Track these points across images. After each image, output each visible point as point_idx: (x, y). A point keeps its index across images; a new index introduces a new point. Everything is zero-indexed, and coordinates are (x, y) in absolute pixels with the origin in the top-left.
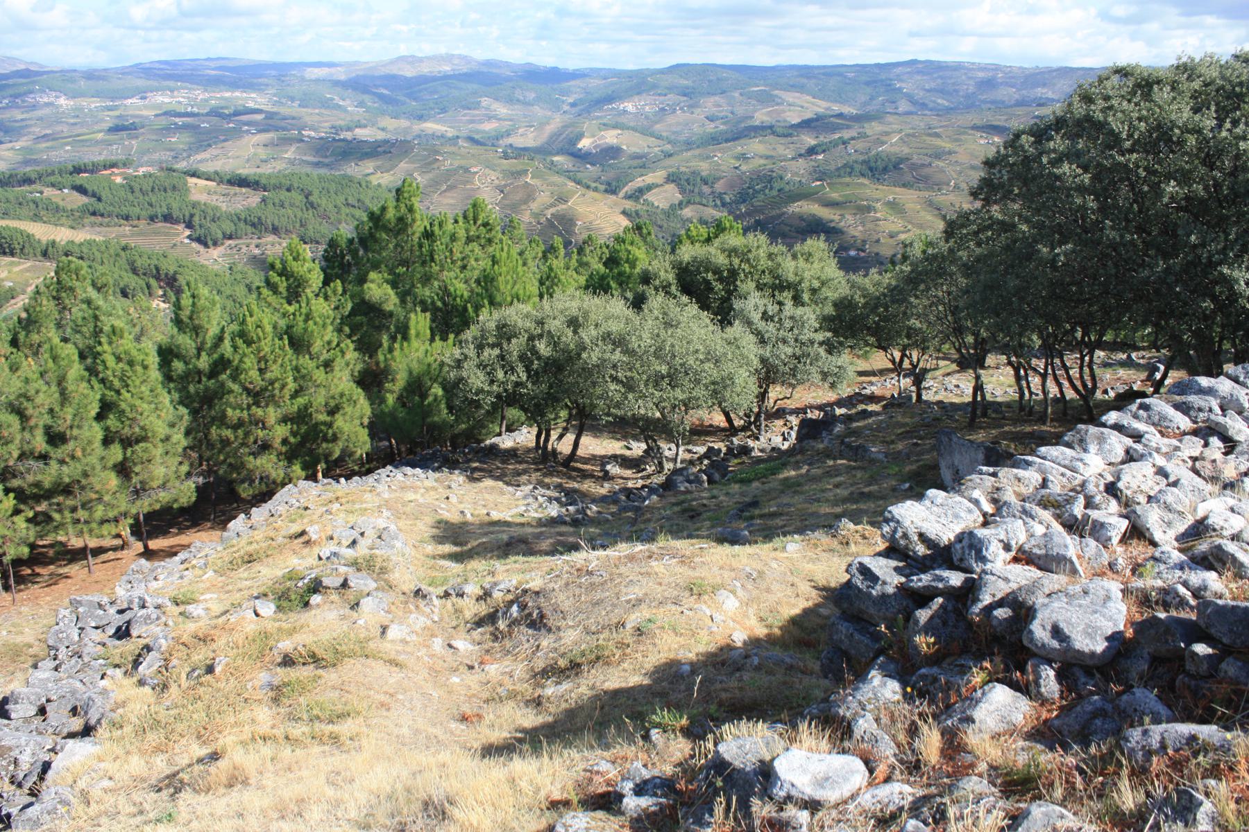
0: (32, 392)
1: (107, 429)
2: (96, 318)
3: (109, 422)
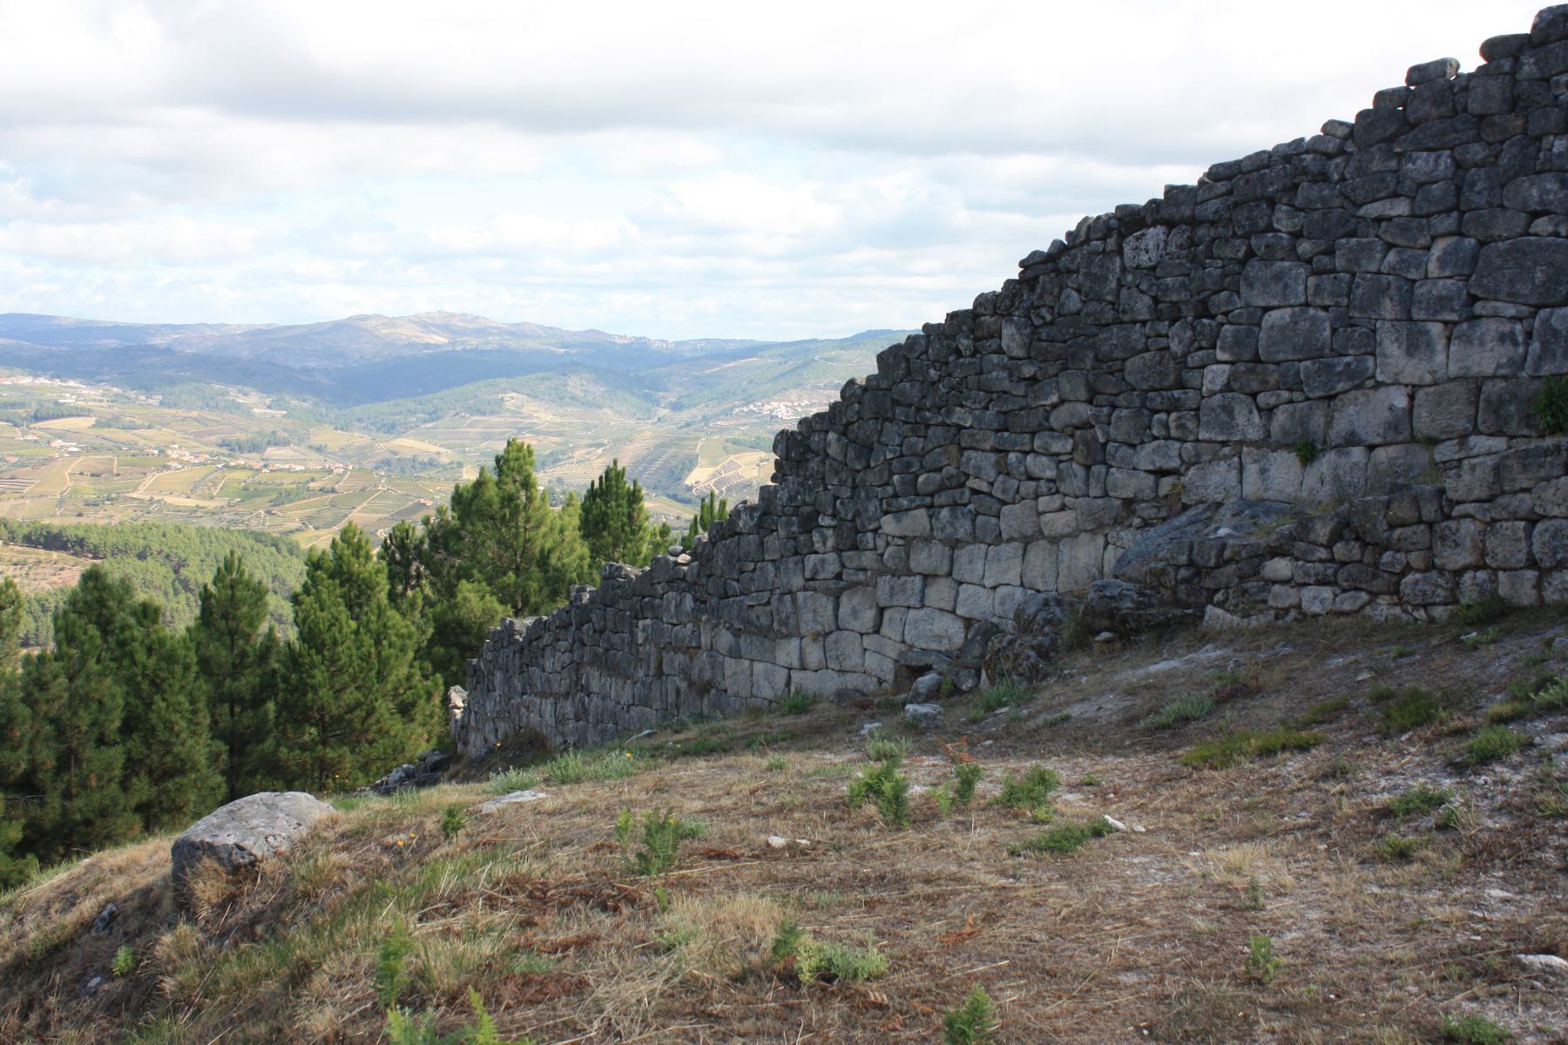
1: (128, 752)
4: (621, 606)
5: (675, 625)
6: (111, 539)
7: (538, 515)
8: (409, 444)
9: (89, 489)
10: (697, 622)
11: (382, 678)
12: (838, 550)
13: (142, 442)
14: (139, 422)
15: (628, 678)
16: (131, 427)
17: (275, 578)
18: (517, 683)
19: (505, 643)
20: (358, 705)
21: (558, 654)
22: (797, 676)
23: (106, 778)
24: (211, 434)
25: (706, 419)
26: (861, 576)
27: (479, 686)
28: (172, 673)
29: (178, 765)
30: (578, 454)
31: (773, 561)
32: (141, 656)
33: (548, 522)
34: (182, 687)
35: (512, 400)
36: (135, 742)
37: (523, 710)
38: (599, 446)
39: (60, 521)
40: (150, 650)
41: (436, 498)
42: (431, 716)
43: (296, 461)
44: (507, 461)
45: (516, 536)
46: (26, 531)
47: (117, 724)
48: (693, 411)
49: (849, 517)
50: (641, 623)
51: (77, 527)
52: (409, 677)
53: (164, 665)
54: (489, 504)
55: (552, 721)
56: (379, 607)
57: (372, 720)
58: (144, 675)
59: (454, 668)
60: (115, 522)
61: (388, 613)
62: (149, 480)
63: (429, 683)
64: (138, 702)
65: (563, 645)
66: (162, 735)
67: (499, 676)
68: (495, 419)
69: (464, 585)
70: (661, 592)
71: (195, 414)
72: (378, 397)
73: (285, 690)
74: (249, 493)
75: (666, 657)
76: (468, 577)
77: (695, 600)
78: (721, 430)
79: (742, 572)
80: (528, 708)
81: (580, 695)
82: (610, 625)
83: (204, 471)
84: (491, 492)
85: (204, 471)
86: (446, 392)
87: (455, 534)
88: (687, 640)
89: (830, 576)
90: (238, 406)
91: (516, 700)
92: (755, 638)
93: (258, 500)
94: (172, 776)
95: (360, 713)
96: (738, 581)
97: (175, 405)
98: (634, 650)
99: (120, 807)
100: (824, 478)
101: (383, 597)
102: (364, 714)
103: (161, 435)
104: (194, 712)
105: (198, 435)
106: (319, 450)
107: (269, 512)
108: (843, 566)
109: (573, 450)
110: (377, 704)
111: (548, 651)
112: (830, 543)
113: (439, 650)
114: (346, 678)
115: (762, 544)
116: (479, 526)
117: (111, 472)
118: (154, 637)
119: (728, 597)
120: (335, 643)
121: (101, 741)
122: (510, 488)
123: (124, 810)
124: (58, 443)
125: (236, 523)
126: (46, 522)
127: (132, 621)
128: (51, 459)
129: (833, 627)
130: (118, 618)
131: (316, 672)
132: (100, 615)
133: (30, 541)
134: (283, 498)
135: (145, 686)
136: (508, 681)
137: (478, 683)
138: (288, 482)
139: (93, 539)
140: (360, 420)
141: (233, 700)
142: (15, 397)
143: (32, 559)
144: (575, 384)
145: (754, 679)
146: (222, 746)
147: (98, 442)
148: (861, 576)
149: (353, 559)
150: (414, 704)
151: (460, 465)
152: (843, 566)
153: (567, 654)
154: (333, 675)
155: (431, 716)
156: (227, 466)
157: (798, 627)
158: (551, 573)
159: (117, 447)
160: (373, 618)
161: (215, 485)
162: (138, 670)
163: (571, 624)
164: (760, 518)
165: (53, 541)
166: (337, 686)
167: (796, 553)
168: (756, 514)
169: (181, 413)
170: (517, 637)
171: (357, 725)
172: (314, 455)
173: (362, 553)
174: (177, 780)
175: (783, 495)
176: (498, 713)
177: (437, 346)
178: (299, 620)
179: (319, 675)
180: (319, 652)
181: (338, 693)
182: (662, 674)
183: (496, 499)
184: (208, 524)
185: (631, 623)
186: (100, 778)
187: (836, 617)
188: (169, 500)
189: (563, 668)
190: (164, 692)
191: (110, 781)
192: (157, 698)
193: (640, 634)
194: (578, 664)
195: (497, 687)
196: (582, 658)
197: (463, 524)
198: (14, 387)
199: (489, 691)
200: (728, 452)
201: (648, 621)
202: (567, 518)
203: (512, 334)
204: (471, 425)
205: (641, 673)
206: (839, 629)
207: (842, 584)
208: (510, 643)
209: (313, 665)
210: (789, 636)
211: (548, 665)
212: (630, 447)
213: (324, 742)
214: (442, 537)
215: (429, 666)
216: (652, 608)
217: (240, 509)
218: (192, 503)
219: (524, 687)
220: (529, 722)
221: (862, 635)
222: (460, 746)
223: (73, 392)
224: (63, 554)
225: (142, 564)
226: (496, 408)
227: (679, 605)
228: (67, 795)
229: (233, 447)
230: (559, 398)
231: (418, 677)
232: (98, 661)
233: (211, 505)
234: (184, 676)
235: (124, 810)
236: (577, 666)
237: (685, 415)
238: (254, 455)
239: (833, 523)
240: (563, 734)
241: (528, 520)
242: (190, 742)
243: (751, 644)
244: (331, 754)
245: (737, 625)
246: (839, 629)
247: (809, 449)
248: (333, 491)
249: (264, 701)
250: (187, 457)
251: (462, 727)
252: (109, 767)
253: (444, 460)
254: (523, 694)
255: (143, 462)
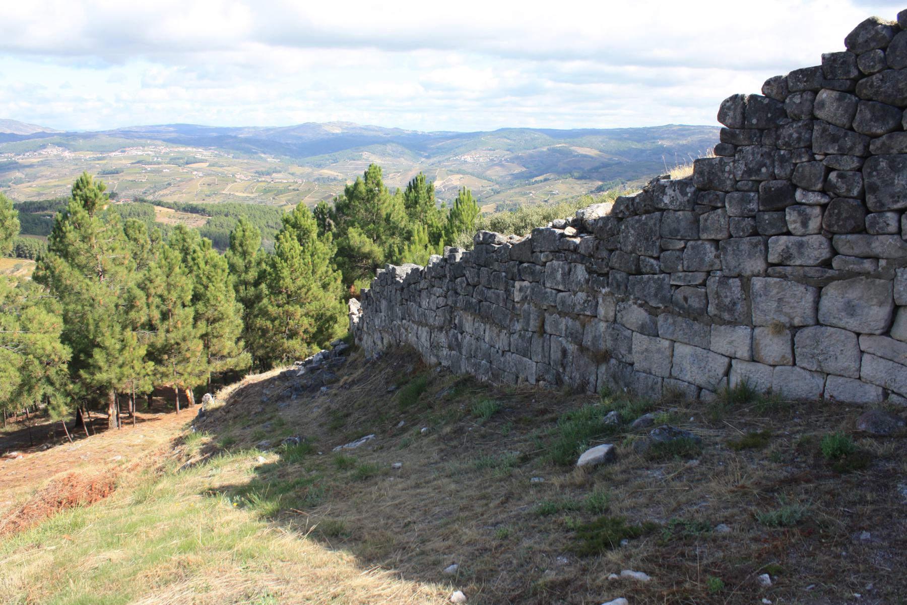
0: (153, 277)
1: (196, 312)
2: (184, 240)
3: (198, 306)
4: (496, 268)
5: (560, 291)
6: (215, 209)
7: (383, 198)
8: (326, 172)
9: (207, 190)
10: (593, 293)
11: (314, 272)
12: (828, 233)
13: (226, 172)
14: (225, 164)
15: (504, 328)
16: (222, 166)
17: (276, 223)
18: (398, 311)
19: (389, 282)
20: (304, 286)
21: (433, 297)
22: (740, 370)
23: (186, 323)
24: (252, 168)
25: (439, 162)
26: (868, 265)
27: (370, 307)
28: (217, 273)
29: (220, 316)
30: (391, 175)
31: (716, 242)
32: (202, 265)
33: (388, 201)
34: (221, 280)
35: (365, 155)
36: (200, 306)
37: (403, 330)
38: (399, 172)
39: (195, 202)
40: (206, 263)
41: (338, 192)
42: (337, 288)
43: (283, 179)
44: (369, 173)
45: (374, 207)
46: (183, 206)
47: (190, 297)
48: (435, 159)
49: (855, 192)
50: (517, 284)
51: (202, 204)
52: (327, 272)
53: (213, 269)
54: (361, 192)
55: (427, 344)
56: (313, 240)
57: (310, 293)
58: (204, 274)
59: (347, 266)
60: (216, 202)
61: (317, 242)
62: (229, 187)
63: (335, 274)
64: (201, 287)
65: (438, 291)
66: (212, 302)
67: (384, 304)
68: (359, 162)
69: (351, 229)
70: (543, 260)
71: (246, 161)
72: (315, 154)
73: (270, 279)
74: (266, 191)
75: (549, 319)
76: (353, 225)
77: (590, 271)
78: (446, 166)
79: (662, 250)
80: (406, 330)
81: (452, 331)
82: (484, 281)
83: (249, 183)
84: (362, 188)
85: (249, 183)
86: (340, 152)
87: (347, 206)
88: (578, 308)
89: (811, 262)
90: (262, 158)
91: (397, 322)
92: (680, 318)
93: (269, 194)
94: (218, 321)
95: (304, 290)
96: (658, 258)
97: (238, 158)
98: (510, 305)
99: (192, 337)
100: (809, 147)
101: (314, 235)
102: (306, 290)
103: (233, 169)
104: (228, 291)
105: (247, 169)
106: (293, 174)
107: (274, 198)
108: (835, 252)
109: (389, 174)
110: (312, 286)
111: (424, 293)
112: (814, 224)
113: (340, 259)
114: (298, 273)
115: (697, 221)
116: (357, 203)
117: (214, 183)
118: (208, 256)
119: (642, 274)
120: (293, 258)
121: (184, 306)
122: (371, 186)
123: (195, 337)
124: (195, 173)
125: (261, 202)
126: (191, 203)
127: (198, 249)
128: (192, 179)
129: (811, 321)
130: (191, 247)
131: (284, 271)
132: (184, 246)
133: (185, 210)
134: (279, 193)
135: (205, 280)
136: (391, 308)
137: (369, 304)
138: (281, 187)
139: (208, 209)
140: (308, 163)
141: (246, 283)
142: (179, 156)
143: (186, 217)
144: (389, 148)
145: (676, 360)
146: (241, 306)
147: (210, 172)
148: (868, 265)
149: (302, 218)
150: (329, 284)
151: (346, 180)
152: (835, 252)
153: (441, 299)
154: (292, 272)
155: (337, 288)
156: (258, 181)
157: (749, 315)
158: (391, 225)
159: (216, 174)
160: (310, 245)
161: (253, 188)
162: (201, 272)
163: (445, 276)
164: (695, 193)
165: (193, 210)
166: (294, 278)
167: (755, 233)
168: (690, 190)
169: (240, 161)
170: (398, 279)
171: (303, 295)
172: (291, 176)
173: (306, 216)
174: (220, 323)
175: (736, 168)
176: (383, 327)
177: (337, 134)
178: (276, 247)
179: (286, 273)
180: (286, 261)
181: (294, 281)
182: (545, 332)
183: (364, 191)
184: (251, 202)
185: (507, 283)
186: (183, 323)
187: (816, 309)
188: (237, 194)
189: (438, 308)
190: (213, 282)
191: (187, 324)
192: (210, 284)
193: (516, 293)
194: (451, 307)
195: (383, 310)
196: (456, 303)
197: (350, 202)
198: (179, 152)
199: (376, 311)
200: (448, 175)
201: (526, 283)
202: (396, 200)
203: (365, 129)
204: (350, 165)
205: (518, 327)
206: (818, 323)
207: (830, 273)
208: (392, 282)
209: (283, 268)
210: (734, 323)
211: (424, 303)
212: (410, 173)
213: (288, 303)
214: (341, 208)
215: (335, 267)
216: (533, 273)
217: (263, 197)
218: (245, 195)
219: (403, 314)
220: (407, 339)
221: (858, 335)
222: (356, 340)
223: (200, 153)
224: (197, 215)
225: (227, 218)
226: (360, 158)
227: (568, 274)
228: (168, 331)
229: (260, 174)
230: (383, 154)
231: (331, 271)
232: (180, 268)
233: (252, 196)
234: (222, 275)
235: (195, 337)
236: (452, 309)
237: (431, 161)
238: (268, 176)
239: (824, 200)
240: (437, 356)
241: (379, 201)
242: (226, 305)
243: (674, 323)
244: (291, 309)
245: (653, 303)
246: (818, 323)
247: (784, 114)
248: (298, 190)
249: (260, 283)
250: (243, 178)
251: (358, 329)
252: (187, 318)
253: (340, 178)
254: (403, 319)
255: (227, 179)
